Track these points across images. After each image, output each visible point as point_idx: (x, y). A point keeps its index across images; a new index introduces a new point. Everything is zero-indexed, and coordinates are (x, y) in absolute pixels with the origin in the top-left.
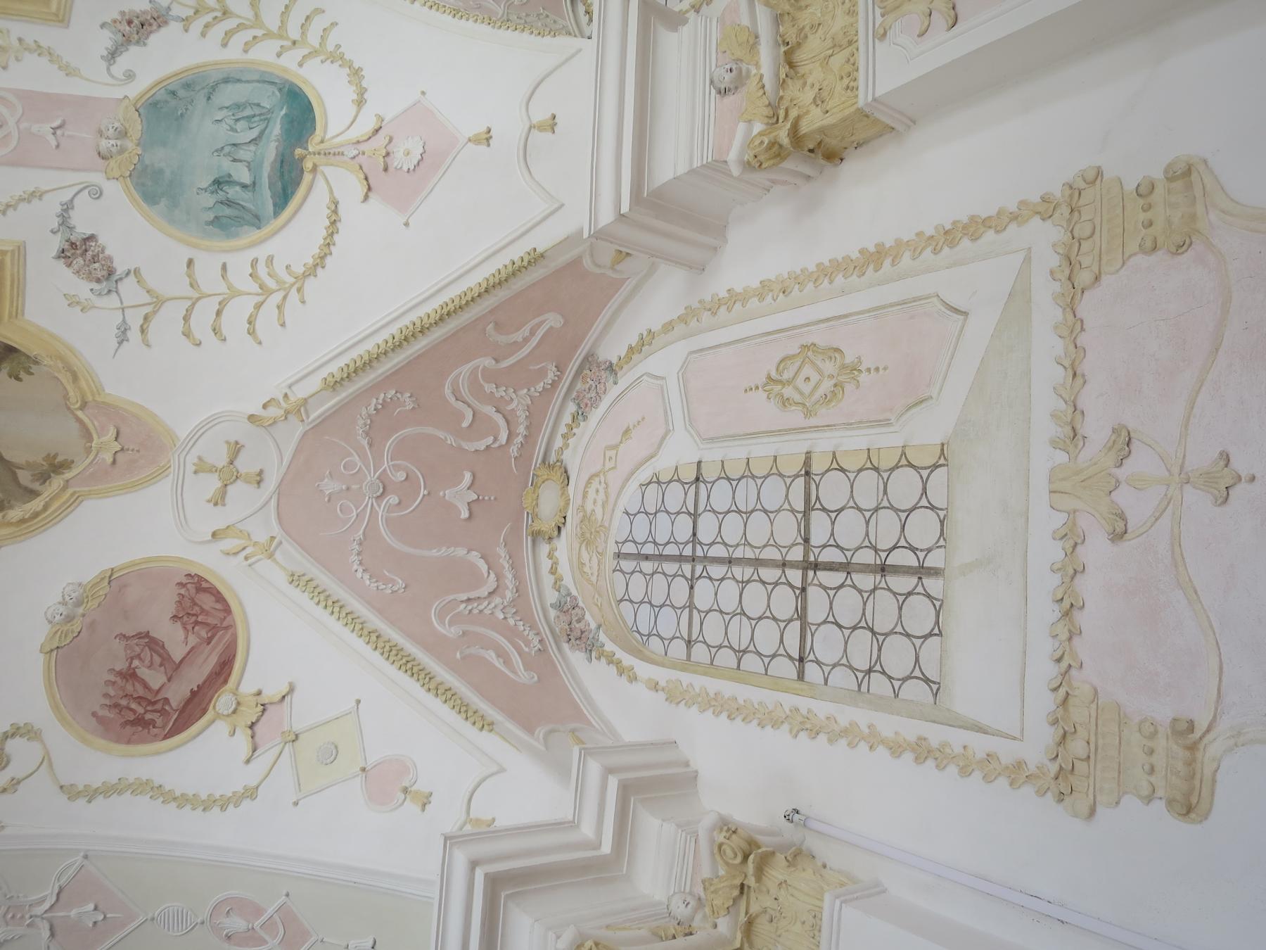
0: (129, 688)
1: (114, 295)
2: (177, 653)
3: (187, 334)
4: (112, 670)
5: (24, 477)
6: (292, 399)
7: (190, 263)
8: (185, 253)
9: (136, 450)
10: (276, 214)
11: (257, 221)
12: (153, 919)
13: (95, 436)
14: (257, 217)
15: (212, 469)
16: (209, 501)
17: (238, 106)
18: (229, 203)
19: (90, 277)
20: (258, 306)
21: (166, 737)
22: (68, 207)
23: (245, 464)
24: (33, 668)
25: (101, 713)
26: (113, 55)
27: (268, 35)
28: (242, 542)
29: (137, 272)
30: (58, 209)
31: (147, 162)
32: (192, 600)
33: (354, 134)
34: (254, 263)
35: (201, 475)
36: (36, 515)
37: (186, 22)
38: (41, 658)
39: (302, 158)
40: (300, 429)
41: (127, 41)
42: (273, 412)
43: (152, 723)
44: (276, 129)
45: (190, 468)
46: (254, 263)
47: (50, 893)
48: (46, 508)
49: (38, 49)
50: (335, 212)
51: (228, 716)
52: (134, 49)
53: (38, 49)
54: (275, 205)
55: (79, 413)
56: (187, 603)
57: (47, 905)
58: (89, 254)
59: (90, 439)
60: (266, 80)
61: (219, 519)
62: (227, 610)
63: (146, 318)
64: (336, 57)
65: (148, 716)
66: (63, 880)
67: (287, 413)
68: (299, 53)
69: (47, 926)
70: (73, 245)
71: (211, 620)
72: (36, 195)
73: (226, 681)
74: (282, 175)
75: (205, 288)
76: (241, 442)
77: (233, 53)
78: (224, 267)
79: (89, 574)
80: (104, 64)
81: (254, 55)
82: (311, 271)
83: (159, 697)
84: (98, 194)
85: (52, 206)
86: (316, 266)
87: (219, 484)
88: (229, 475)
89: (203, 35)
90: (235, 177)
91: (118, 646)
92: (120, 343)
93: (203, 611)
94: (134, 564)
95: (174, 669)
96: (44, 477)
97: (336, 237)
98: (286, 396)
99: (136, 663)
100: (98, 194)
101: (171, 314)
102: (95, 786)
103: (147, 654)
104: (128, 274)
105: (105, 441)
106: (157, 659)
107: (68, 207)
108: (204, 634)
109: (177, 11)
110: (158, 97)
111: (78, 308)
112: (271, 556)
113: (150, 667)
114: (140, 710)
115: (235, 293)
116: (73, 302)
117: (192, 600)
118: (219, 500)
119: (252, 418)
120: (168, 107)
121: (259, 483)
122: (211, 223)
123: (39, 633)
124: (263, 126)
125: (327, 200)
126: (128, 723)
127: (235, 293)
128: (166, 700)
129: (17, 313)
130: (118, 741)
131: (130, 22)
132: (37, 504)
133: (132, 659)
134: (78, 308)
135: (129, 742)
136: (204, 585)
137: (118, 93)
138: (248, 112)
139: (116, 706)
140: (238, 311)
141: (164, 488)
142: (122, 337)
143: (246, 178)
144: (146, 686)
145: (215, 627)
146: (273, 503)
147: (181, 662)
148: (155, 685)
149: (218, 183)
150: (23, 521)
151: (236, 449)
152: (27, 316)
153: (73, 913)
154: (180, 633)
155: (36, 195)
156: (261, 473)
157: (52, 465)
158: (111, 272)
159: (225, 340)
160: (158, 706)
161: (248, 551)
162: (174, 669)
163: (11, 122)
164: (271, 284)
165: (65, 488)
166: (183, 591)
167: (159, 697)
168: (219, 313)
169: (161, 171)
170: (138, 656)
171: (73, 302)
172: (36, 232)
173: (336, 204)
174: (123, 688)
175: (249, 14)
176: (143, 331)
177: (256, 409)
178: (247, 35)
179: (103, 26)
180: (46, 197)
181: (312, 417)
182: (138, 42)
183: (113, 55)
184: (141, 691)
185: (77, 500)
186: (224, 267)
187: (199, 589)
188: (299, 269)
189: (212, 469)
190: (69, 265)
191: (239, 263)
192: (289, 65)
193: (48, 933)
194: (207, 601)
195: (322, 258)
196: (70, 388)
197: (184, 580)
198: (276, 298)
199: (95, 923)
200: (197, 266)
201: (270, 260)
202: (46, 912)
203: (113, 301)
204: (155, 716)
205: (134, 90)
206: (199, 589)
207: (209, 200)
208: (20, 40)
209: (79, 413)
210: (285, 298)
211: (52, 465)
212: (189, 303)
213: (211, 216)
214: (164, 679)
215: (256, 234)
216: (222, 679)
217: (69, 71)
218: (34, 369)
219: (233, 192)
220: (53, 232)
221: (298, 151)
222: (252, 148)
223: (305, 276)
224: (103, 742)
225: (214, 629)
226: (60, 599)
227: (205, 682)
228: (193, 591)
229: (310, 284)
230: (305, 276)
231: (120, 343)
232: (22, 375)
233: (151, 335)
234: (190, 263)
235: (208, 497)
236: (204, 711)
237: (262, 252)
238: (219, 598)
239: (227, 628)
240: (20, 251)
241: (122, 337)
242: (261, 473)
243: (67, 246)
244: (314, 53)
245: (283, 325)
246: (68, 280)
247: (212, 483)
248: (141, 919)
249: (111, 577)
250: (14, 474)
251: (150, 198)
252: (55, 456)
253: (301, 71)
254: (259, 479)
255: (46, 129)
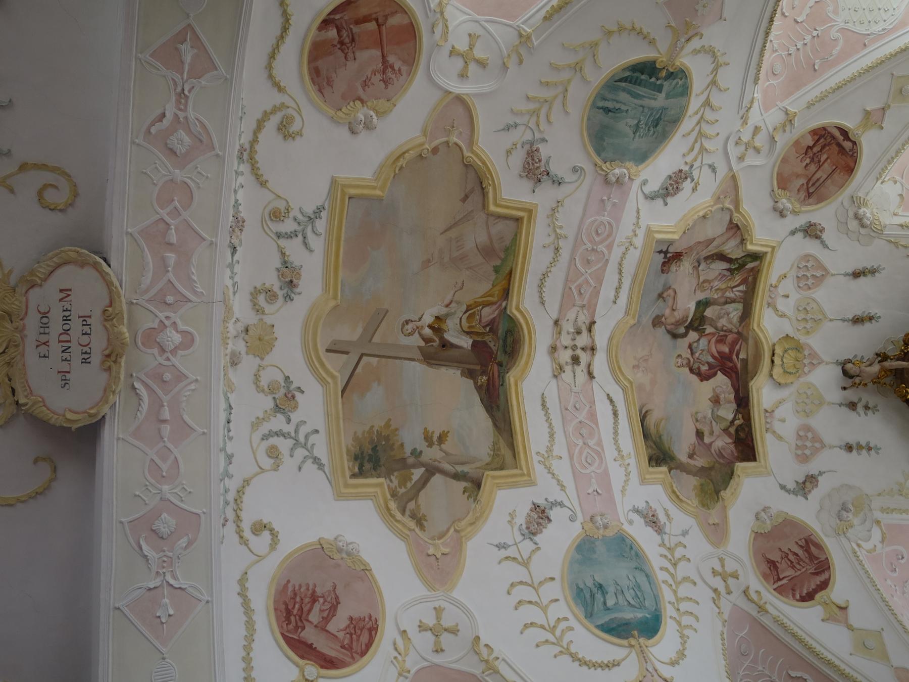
0: (307, 600)
1: (522, 538)
2: (331, 627)
3: (512, 585)
4: (315, 586)
5: (411, 505)
6: (496, 663)
7: (552, 579)
8: (556, 574)
9: (438, 568)
10: (598, 627)
11: (589, 615)
12: (164, 659)
13: (441, 541)
14: (591, 615)
15: (438, 618)
16: (420, 621)
17: (639, 587)
18: (592, 596)
19: (529, 523)
20: (542, 627)
21: (282, 634)
22: (561, 504)
23: (446, 638)
24: (309, 537)
25: (290, 585)
26: (637, 511)
27: (675, 592)
28: (402, 651)
29: (539, 548)
30: (559, 500)
31: (597, 543)
32: (363, 628)
33: (659, 666)
34: (566, 619)
35: (434, 612)
36: (393, 516)
37: (662, 545)
38: (315, 539)
39: (633, 636)
40: (477, 672)
41: (645, 517)
42: (484, 652)
43: (289, 623)
44: (640, 615)
45: (437, 604)
46: (566, 619)
47: (182, 583)
48: (397, 521)
49: (628, 474)
50: (614, 665)
51: (304, 676)
52: (642, 520)
53: (628, 474)
54: (602, 625)
55: (452, 530)
56: (361, 624)
57: (172, 582)
58: (541, 521)
59: (440, 538)
60: (656, 599)
61: (413, 632)
62: (363, 654)
63: (514, 559)
64: (684, 638)
65: (292, 618)
66: (190, 590)
67: (487, 661)
68: (675, 614)
69: (158, 584)
70: (543, 512)
71: (354, 644)
72: (563, 488)
73: (322, 667)
74: (619, 626)
75: (542, 590)
76: (459, 633)
77: (661, 576)
78: (557, 600)
79: (365, 556)
80: (631, 508)
81: (663, 586)
82: (574, 657)
83: (305, 622)
84: (572, 519)
85: (560, 496)
86: (579, 660)
87: (431, 625)
88: (436, 631)
89: (661, 556)
90: (607, 597)
91: (329, 586)
92: (497, 546)
93: (359, 636)
94: (376, 582)
95: (322, 627)
96: (413, 516)
97: (599, 669)
98: (498, 658)
99: (321, 600)
100: (572, 519)
101: (520, 573)
102: (248, 594)
103: (327, 606)
104: (536, 544)
105: (443, 547)
106: (325, 614)
107: (561, 504)
108: (346, 642)
109: (666, 537)
110: (627, 540)
111: (509, 519)
112: (400, 675)
113: (321, 611)
114: (295, 612)
115: (545, 609)
116: (512, 515)
117: (363, 628)
118: (422, 628)
119: (477, 638)
120: (624, 547)
121: (437, 651)
122: (578, 587)
123: (329, 535)
124: (637, 606)
125: (618, 658)
126: (286, 605)
127: (545, 609)
128: (303, 628)
129: (500, 487)
130: (275, 602)
131: (653, 516)
132: (399, 516)
133: (323, 597)
134: (509, 519)
135: (276, 610)
136: (373, 633)
137: (622, 520)
138: (639, 593)
139: (295, 594)
140: (532, 614)
141: (420, 590)
142: (500, 546)
143: (610, 602)
144: (310, 611)
145: (352, 648)
146: (426, 664)
147: (327, 631)
148: (311, 618)
149: (600, 587)
150: (388, 509)
151: (454, 631)
152: (499, 492)
153: (166, 600)
154: (343, 626)
155: (563, 488)
156: (442, 650)
157: (421, 519)
158: (534, 534)
159: (516, 609)
160: (300, 624)
161: (399, 657)
162: (322, 627)
163: (593, 468)
164: (558, 632)
165: (410, 530)
166: (367, 619)
167: (305, 622)
168: (530, 602)
169: (595, 552)
170: (325, 601)
171: (512, 515)
172: (544, 489)
173: (618, 665)
174: (306, 596)
175: (679, 579)
176: (507, 558)
177: (484, 640)
178: (671, 581)
179: (647, 502)
180: (562, 492)
181: (487, 678)
182: (646, 522)
183: (637, 511)
184: (306, 609)
185: (403, 537)
186: (557, 600)
187: (370, 630)
188: (573, 650)
189: (438, 618)
190: (531, 510)
191: (562, 609)
192: (669, 611)
193: (152, 587)
194: (364, 638)
195: (586, 663)
196: (463, 523)
197: (373, 619)
198: (551, 638)
199: (159, 617)
200: (550, 584)
201: (571, 629)
202: (168, 582)
203: (519, 538)
204: (293, 623)
205: (626, 527)
206: (370, 630)
207: (590, 583)
208: (629, 464)
209: (452, 530)
210: (553, 643)
211: (421, 519)
212: (530, 582)
213: (582, 586)
214: (315, 623)
215: (582, 616)
216: (323, 663)
217: (623, 491)
218: (471, 500)
219: (599, 596)
220: (546, 499)
221: (636, 633)
222: (626, 603)
223: (571, 655)
224: (273, 592)
225: (349, 648)
226: (349, 541)
227: (319, 652)
228: (368, 626)
229: (566, 658)
230: (571, 655)
231: (497, 546)
232: (466, 494)
233: (505, 563)
234: (552, 579)
235: (423, 621)
236: (302, 657)
237: (573, 622)
238: (369, 645)
239: (353, 658)
240: (532, 483)
241: (500, 546)
242: (442, 650)
243: (542, 508)
244: (679, 623)
245: (537, 646)
246: (523, 512)
247: (430, 621)
248: (164, 650)
249: (367, 569)
250: (411, 500)
251: (579, 548)
252: (426, 520)
253: (669, 620)
254: (438, 650)
255: (596, 487)
